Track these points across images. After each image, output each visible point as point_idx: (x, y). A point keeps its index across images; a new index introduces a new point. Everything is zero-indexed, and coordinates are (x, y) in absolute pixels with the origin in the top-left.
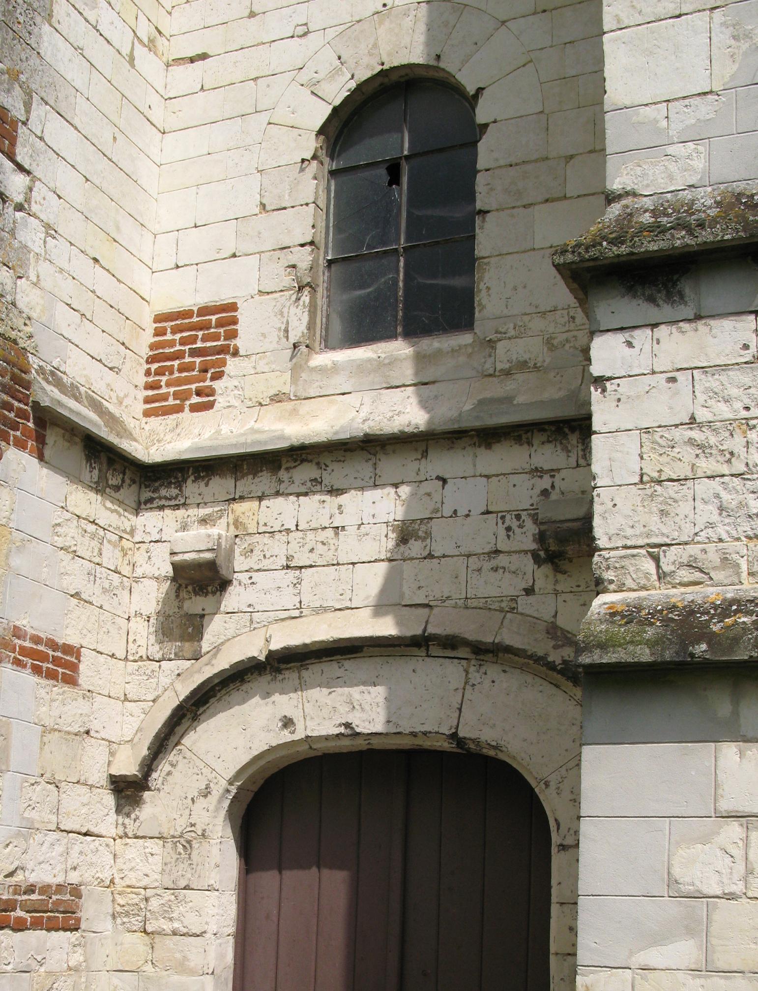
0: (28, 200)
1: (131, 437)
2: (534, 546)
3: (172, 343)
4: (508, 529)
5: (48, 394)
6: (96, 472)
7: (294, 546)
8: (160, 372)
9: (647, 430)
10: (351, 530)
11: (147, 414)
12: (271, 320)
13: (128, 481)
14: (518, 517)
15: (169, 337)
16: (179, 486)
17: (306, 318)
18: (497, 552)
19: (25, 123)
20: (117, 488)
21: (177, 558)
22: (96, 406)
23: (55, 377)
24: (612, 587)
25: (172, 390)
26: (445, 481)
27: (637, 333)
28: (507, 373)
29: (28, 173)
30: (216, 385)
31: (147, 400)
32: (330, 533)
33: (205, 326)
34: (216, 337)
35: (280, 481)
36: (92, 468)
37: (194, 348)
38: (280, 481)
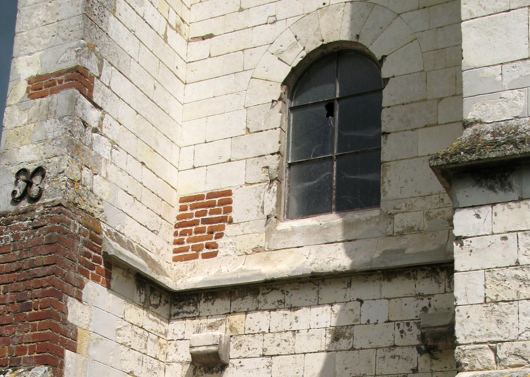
0: (100, 126)
1: (165, 274)
2: (418, 342)
3: (191, 216)
4: (402, 332)
5: (113, 247)
6: (143, 296)
7: (267, 342)
8: (183, 234)
9: (489, 270)
10: (303, 333)
11: (175, 260)
12: (253, 201)
13: (163, 302)
14: (408, 324)
15: (189, 211)
16: (195, 305)
17: (275, 200)
18: (395, 346)
19: (98, 78)
20: (156, 306)
21: (194, 350)
22: (143, 255)
23: (117, 237)
24: (467, 368)
25: (191, 245)
26: (362, 302)
27: (483, 209)
28: (401, 234)
29: (101, 109)
30: (219, 242)
31: (175, 251)
32: (290, 334)
33: (212, 205)
34: (218, 212)
35: (259, 302)
36: (141, 294)
37: (204, 219)
38: (259, 302)
